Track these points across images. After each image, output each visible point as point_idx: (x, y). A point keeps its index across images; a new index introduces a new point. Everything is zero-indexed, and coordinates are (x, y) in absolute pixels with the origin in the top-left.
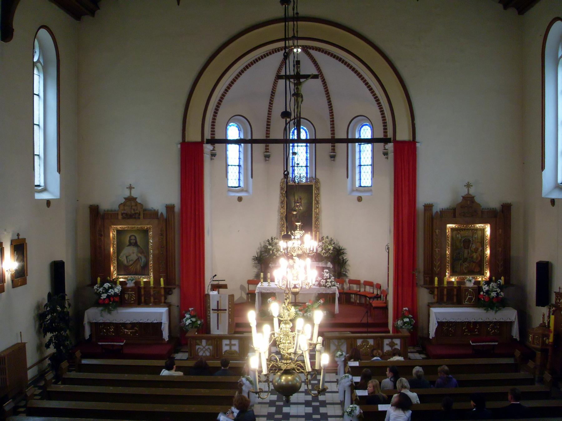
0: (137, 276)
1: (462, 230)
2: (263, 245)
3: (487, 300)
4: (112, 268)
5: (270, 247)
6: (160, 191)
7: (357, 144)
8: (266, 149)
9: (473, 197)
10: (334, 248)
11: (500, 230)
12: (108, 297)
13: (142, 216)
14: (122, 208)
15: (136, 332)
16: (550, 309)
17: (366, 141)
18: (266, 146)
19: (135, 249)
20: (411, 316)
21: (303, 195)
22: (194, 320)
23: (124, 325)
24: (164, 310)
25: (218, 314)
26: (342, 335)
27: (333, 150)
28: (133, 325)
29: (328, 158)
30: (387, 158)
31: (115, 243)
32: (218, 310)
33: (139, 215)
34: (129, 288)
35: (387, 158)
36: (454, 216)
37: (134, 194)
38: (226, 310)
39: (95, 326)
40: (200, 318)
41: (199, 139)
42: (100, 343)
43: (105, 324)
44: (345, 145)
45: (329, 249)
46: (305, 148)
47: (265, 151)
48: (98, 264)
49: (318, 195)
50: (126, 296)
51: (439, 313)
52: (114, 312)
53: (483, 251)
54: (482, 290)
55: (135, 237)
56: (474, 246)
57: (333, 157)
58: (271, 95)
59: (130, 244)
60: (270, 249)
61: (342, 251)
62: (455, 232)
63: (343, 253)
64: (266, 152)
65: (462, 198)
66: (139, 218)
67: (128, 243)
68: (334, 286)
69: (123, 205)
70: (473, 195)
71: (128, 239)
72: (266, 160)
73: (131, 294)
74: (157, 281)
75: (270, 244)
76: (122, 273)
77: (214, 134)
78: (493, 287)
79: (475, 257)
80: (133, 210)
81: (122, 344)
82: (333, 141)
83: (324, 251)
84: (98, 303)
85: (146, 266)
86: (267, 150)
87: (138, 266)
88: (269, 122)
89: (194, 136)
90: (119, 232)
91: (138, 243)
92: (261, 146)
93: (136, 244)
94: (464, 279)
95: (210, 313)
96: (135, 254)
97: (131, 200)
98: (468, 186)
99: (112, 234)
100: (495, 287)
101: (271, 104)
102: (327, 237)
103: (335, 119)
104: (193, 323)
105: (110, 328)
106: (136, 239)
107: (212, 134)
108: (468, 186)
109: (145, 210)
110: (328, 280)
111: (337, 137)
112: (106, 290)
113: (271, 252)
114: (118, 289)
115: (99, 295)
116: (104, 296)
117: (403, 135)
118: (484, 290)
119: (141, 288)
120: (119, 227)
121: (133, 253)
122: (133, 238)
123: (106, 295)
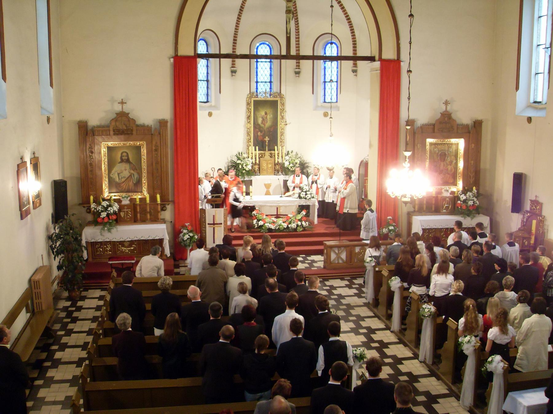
0: (130, 194)
1: (439, 144)
2: (230, 160)
3: (464, 207)
4: (104, 186)
5: (239, 162)
6: (153, 106)
7: (322, 61)
8: (233, 64)
9: (451, 114)
10: (300, 162)
11: (473, 145)
12: (108, 215)
13: (134, 132)
14: (113, 124)
15: (135, 249)
16: (524, 215)
17: (331, 59)
18: (233, 61)
19: (127, 166)
20: (394, 224)
21: (269, 111)
22: (191, 235)
23: (122, 243)
24: (163, 226)
25: (214, 228)
26: (342, 244)
27: (298, 66)
28: (132, 242)
29: (293, 74)
30: (356, 75)
31: (106, 160)
32: (214, 224)
33: (132, 130)
34: (125, 205)
35: (356, 75)
36: (434, 132)
37: (127, 108)
38: (221, 224)
39: (93, 245)
40: (197, 233)
41: (192, 54)
42: (111, 262)
43: (106, 243)
44: (310, 62)
45: (296, 163)
46: (269, 64)
47: (231, 66)
48: (89, 181)
49: (283, 110)
50: (122, 214)
51: (424, 221)
52: (114, 230)
53: (456, 164)
54: (460, 200)
55: (127, 154)
56: (449, 159)
57: (298, 73)
58: (240, 10)
59: (122, 161)
60: (239, 164)
61: (306, 165)
62: (433, 146)
63: (308, 167)
64: (232, 67)
65: (440, 115)
66: (132, 134)
67: (120, 160)
68: (313, 198)
69: (115, 120)
70: (451, 112)
71: (119, 156)
72: (232, 75)
73: (127, 211)
74: (153, 199)
75: (239, 159)
76: (114, 191)
77: (299, 50)
78: (470, 196)
79: (449, 169)
80: (123, 125)
81: (133, 262)
82: (299, 57)
83: (291, 165)
84: (96, 221)
85: (139, 183)
86: (233, 65)
87: (131, 183)
88: (236, 37)
89: (186, 50)
90: (109, 149)
91: (131, 160)
92: (228, 61)
93: (128, 161)
94: (442, 189)
95: (205, 228)
96: (127, 171)
97: (122, 116)
98: (446, 103)
99: (104, 151)
100: (472, 196)
101: (239, 18)
102: (292, 152)
103: (300, 36)
104: (191, 238)
105: (107, 247)
106: (128, 156)
107: (297, 50)
108: (446, 103)
109: (138, 126)
110: (308, 193)
111: (302, 53)
112: (106, 209)
113: (240, 167)
114: (116, 207)
115: (98, 214)
116: (104, 215)
117: (389, 54)
118: (462, 199)
119: (137, 205)
120: (110, 144)
121: (126, 170)
122: (125, 154)
123: (106, 213)
